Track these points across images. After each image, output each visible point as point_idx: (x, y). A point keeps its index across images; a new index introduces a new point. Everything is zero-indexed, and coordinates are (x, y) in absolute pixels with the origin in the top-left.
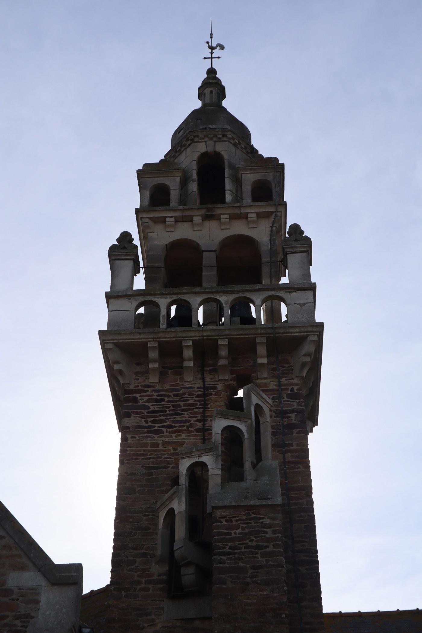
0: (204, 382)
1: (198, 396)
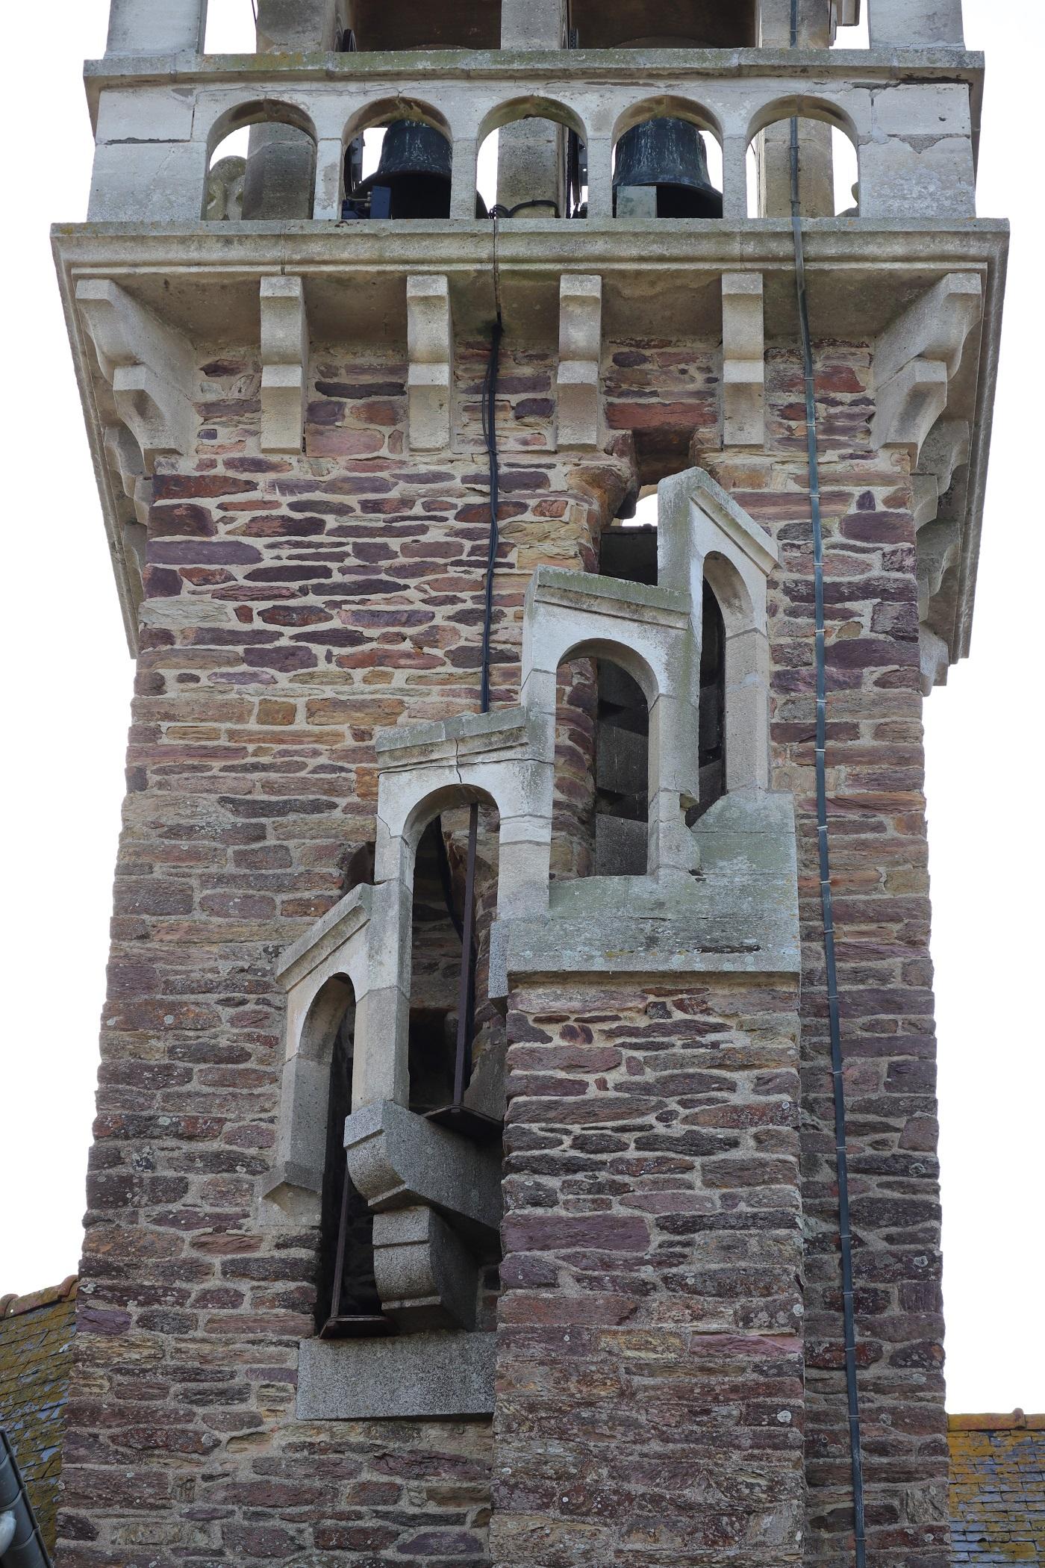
1: (465, 514)
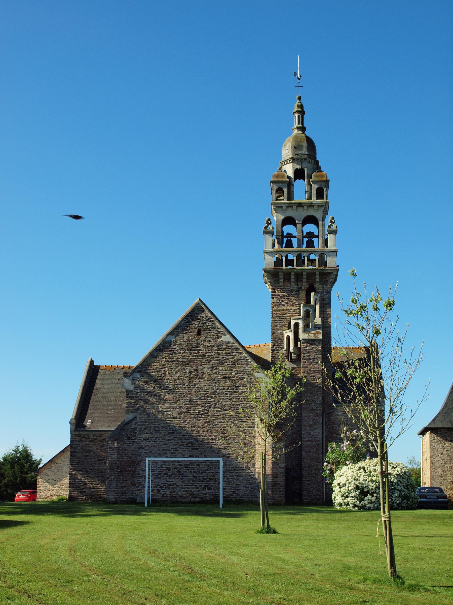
0: (298, 285)
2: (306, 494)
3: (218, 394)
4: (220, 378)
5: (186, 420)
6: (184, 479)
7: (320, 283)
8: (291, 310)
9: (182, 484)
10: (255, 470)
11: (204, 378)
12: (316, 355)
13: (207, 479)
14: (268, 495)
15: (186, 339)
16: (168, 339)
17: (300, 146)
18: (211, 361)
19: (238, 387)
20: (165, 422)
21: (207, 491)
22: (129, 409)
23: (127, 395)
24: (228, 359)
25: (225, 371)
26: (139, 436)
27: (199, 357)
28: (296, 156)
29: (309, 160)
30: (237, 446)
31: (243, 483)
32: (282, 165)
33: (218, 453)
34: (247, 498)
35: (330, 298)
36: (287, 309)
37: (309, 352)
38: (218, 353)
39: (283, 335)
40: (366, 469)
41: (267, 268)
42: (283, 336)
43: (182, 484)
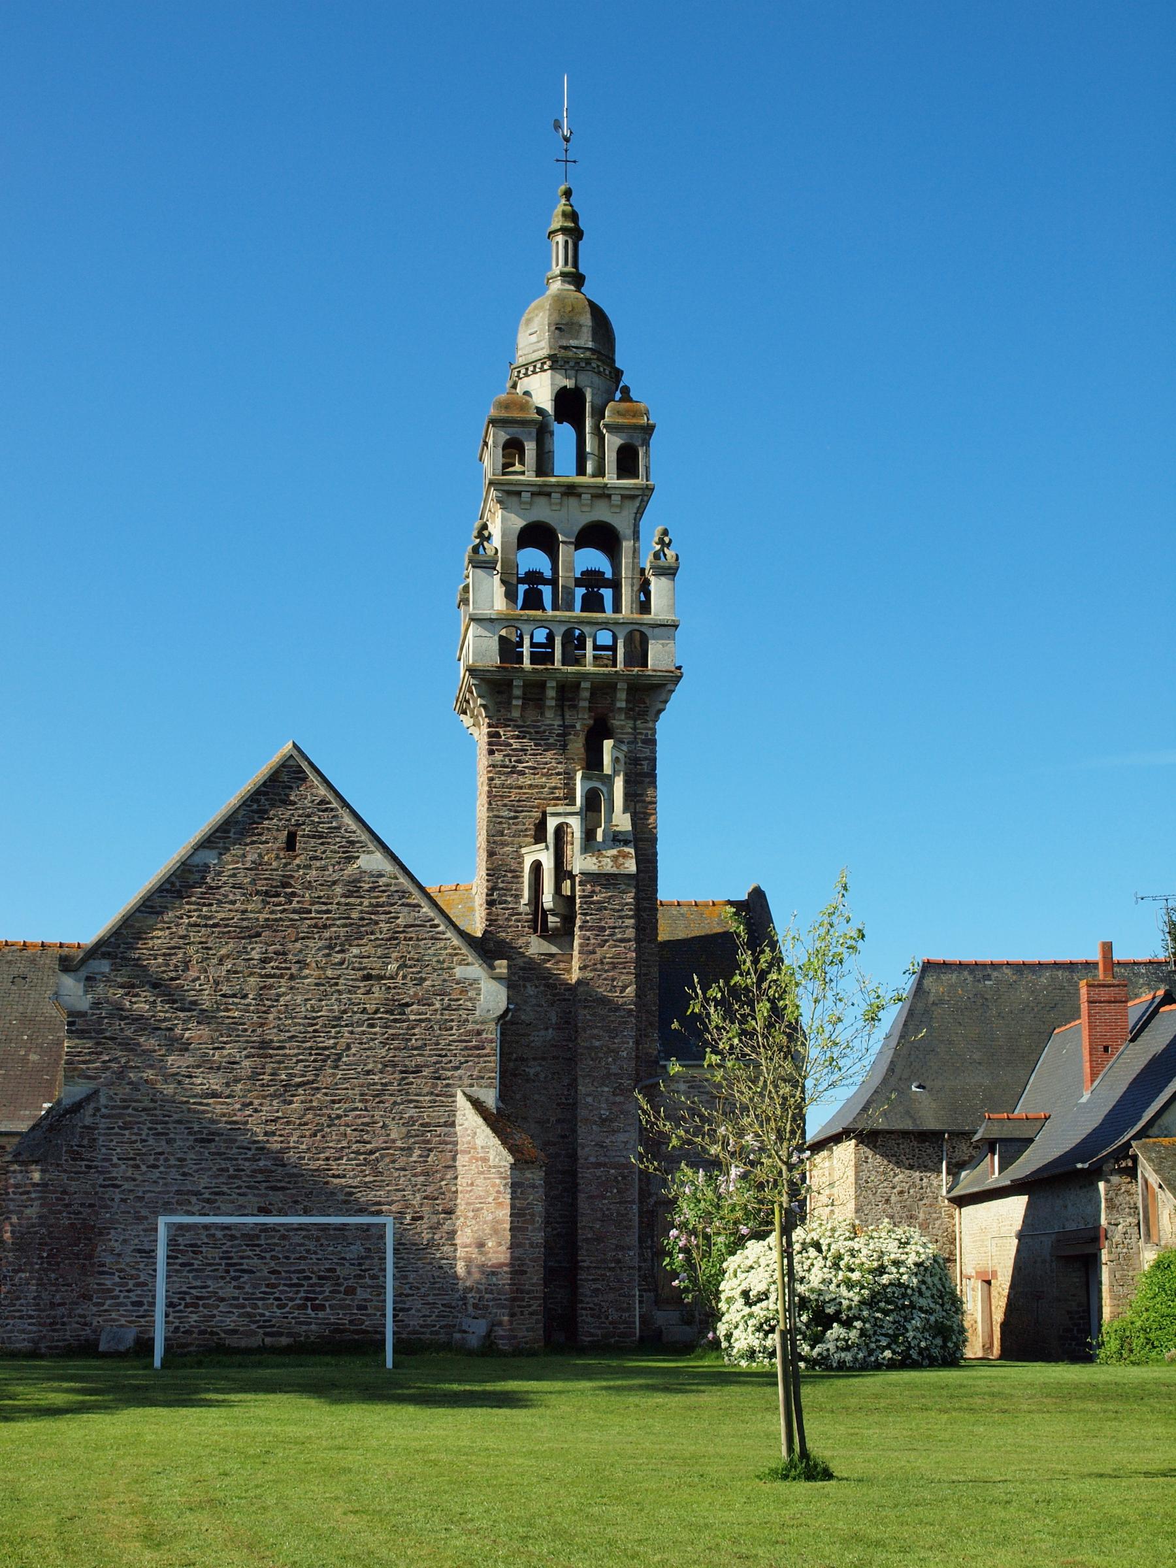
0: (563, 719)
1: (558, 735)
2: (590, 1319)
3: (347, 1026)
4: (352, 980)
5: (251, 1103)
6: (242, 1280)
7: (626, 714)
8: (543, 787)
9: (236, 1293)
10: (456, 1250)
11: (306, 977)
12: (621, 917)
13: (311, 1278)
14: (500, 1324)
15: (253, 862)
16: (198, 859)
17: (572, 324)
18: (325, 927)
19: (407, 1005)
20: (184, 1107)
21: (313, 1314)
22: (75, 1069)
23: (70, 1024)
24: (377, 923)
25: (369, 957)
26: (104, 1150)
27: (292, 916)
28: (563, 353)
29: (598, 366)
30: (403, 1179)
31: (418, 1289)
32: (518, 376)
33: (346, 1202)
34: (432, 1333)
35: (655, 759)
36: (531, 785)
37: (599, 910)
38: (347, 904)
39: (520, 858)
40: (824, 1248)
41: (480, 665)
42: (522, 863)
43: (236, 1293)
